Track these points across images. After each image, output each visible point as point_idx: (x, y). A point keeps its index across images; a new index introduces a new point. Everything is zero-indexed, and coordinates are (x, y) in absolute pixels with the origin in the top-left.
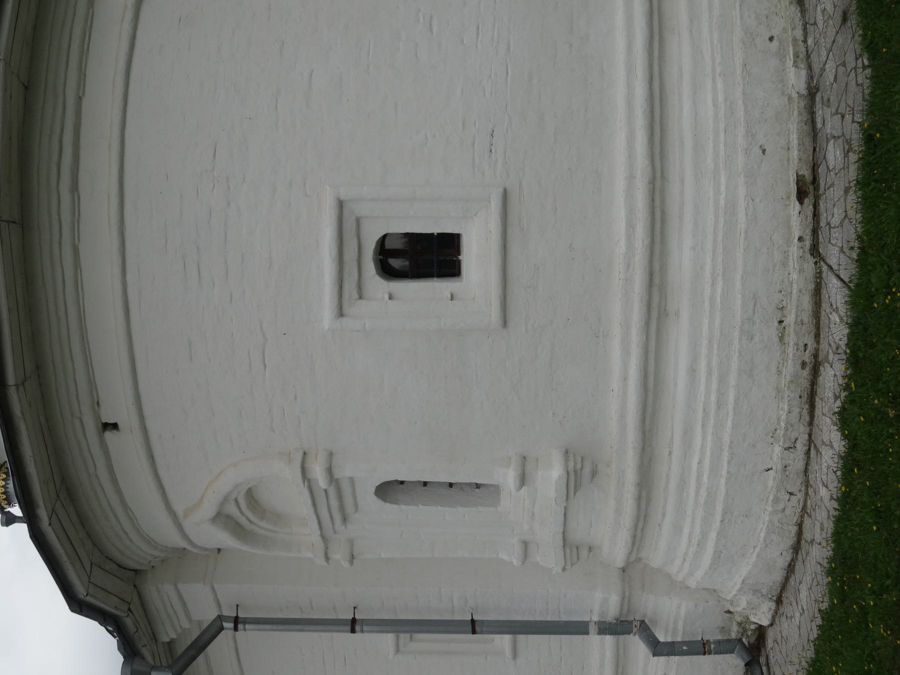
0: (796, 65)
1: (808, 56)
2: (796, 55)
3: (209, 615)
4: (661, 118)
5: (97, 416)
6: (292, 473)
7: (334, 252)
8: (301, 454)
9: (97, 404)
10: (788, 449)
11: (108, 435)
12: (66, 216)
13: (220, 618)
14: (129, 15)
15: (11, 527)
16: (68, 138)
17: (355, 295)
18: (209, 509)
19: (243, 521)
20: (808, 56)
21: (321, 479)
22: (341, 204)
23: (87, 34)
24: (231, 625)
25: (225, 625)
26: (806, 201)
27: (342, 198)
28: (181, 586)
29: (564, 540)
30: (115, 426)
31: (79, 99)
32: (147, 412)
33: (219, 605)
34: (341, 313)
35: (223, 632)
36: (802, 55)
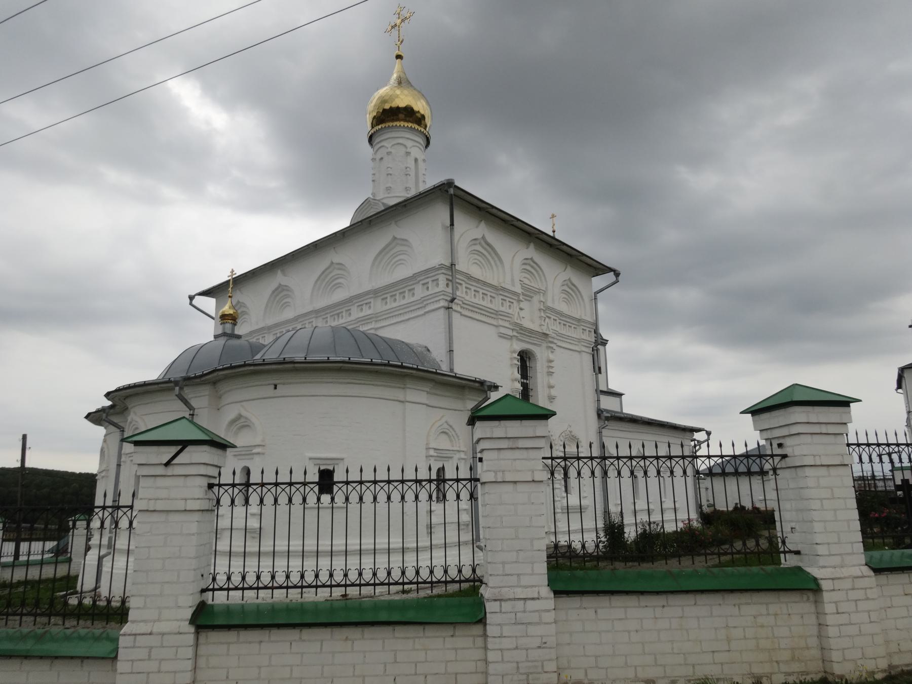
0: (380, 592)
1: (382, 595)
2: (382, 592)
3: (193, 403)
4: (565, 341)
5: (279, 384)
6: (258, 441)
7: (329, 457)
8: (264, 444)
9: (284, 384)
10: (263, 598)
11: (273, 386)
12: (341, 381)
13: (194, 409)
14: (396, 399)
15: (188, 299)
16: (363, 382)
17: (316, 463)
18: (244, 413)
19: (237, 423)
20: (382, 595)
21: (256, 450)
22: (342, 459)
23: (390, 387)
24: (191, 413)
25: (192, 411)
26: (341, 597)
27: (345, 460)
28: (207, 397)
29: (224, 529)
30: (275, 388)
31: (373, 385)
32: (280, 398)
33: (198, 408)
34: (310, 459)
35: (188, 410)
36: (382, 594)
